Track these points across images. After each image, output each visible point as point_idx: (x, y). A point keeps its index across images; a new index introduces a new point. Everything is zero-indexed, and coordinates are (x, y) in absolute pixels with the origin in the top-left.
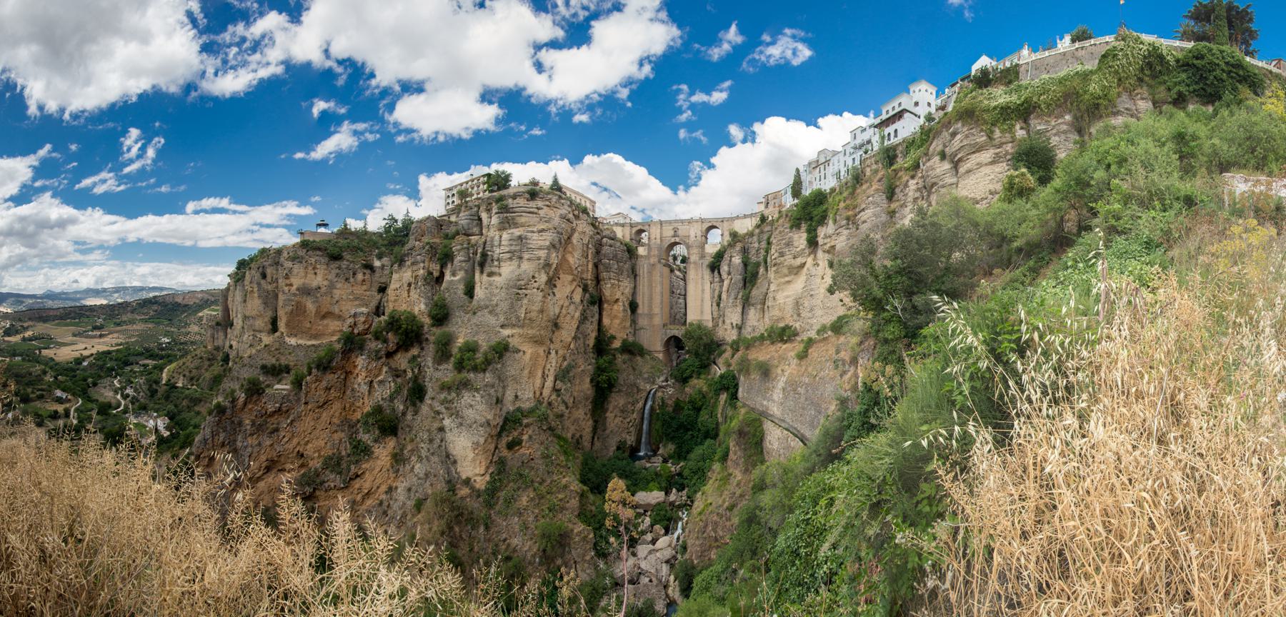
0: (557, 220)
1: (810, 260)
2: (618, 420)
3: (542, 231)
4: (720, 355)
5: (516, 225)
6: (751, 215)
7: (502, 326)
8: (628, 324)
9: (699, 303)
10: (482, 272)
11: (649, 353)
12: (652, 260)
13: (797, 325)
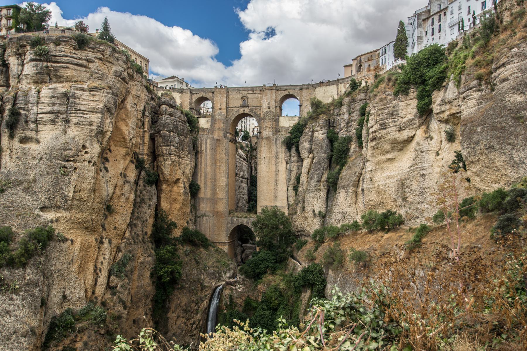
0: (111, 79)
1: (420, 134)
2: (181, 321)
3: (95, 89)
4: (299, 248)
5: (59, 79)
6: (337, 82)
7: (43, 209)
8: (188, 210)
9: (272, 186)
10: (12, 137)
11: (213, 244)
12: (216, 135)
13: (402, 212)
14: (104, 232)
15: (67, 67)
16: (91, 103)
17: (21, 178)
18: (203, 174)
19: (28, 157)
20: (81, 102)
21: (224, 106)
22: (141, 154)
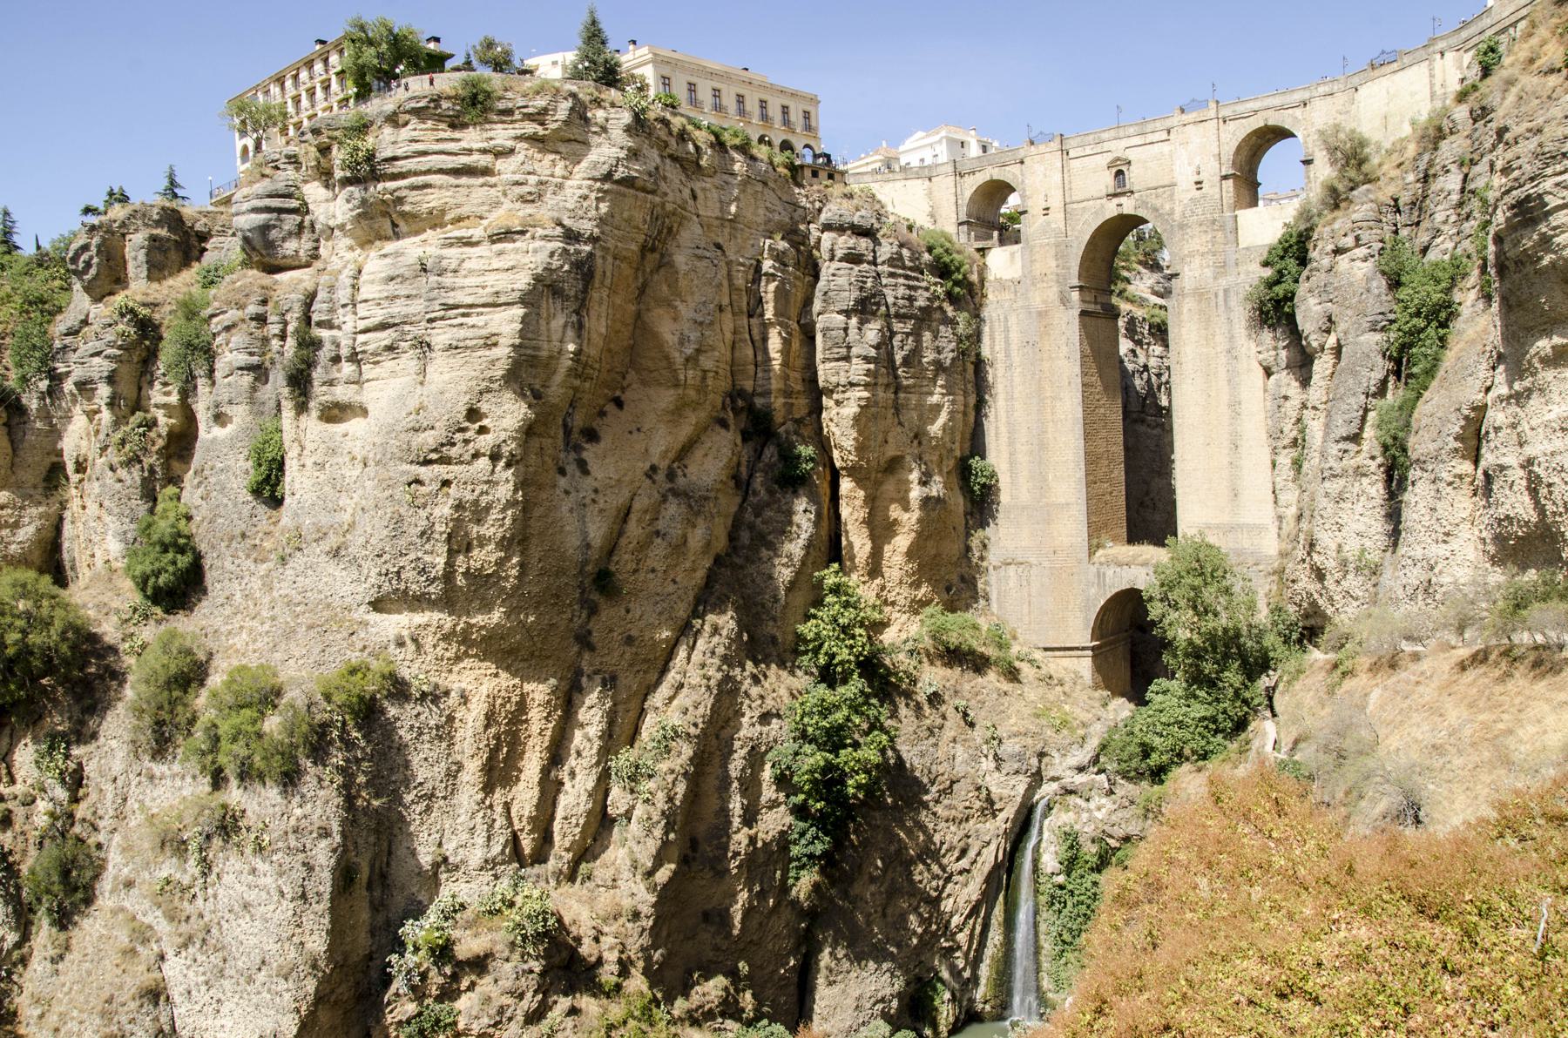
3: (506, 235)
7: (378, 605)
10: (301, 408)
14: (587, 656)
16: (490, 279)
17: (325, 520)
18: (1003, 429)
19: (340, 460)
20: (460, 281)
21: (1056, 203)
22: (761, 395)
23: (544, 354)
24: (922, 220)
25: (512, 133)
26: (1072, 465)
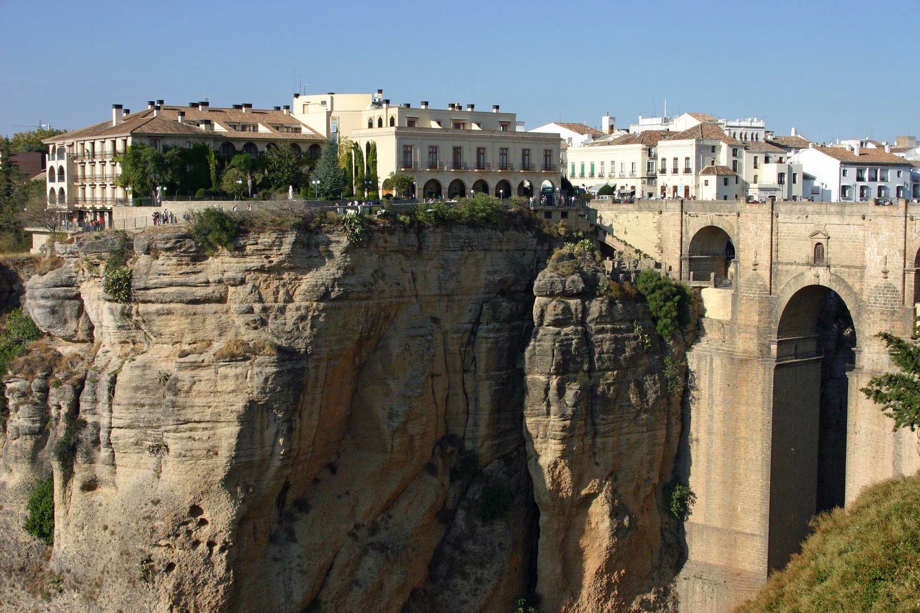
15: (169, 313)
23: (257, 458)
24: (649, 249)
25: (243, 266)
26: (759, 502)
